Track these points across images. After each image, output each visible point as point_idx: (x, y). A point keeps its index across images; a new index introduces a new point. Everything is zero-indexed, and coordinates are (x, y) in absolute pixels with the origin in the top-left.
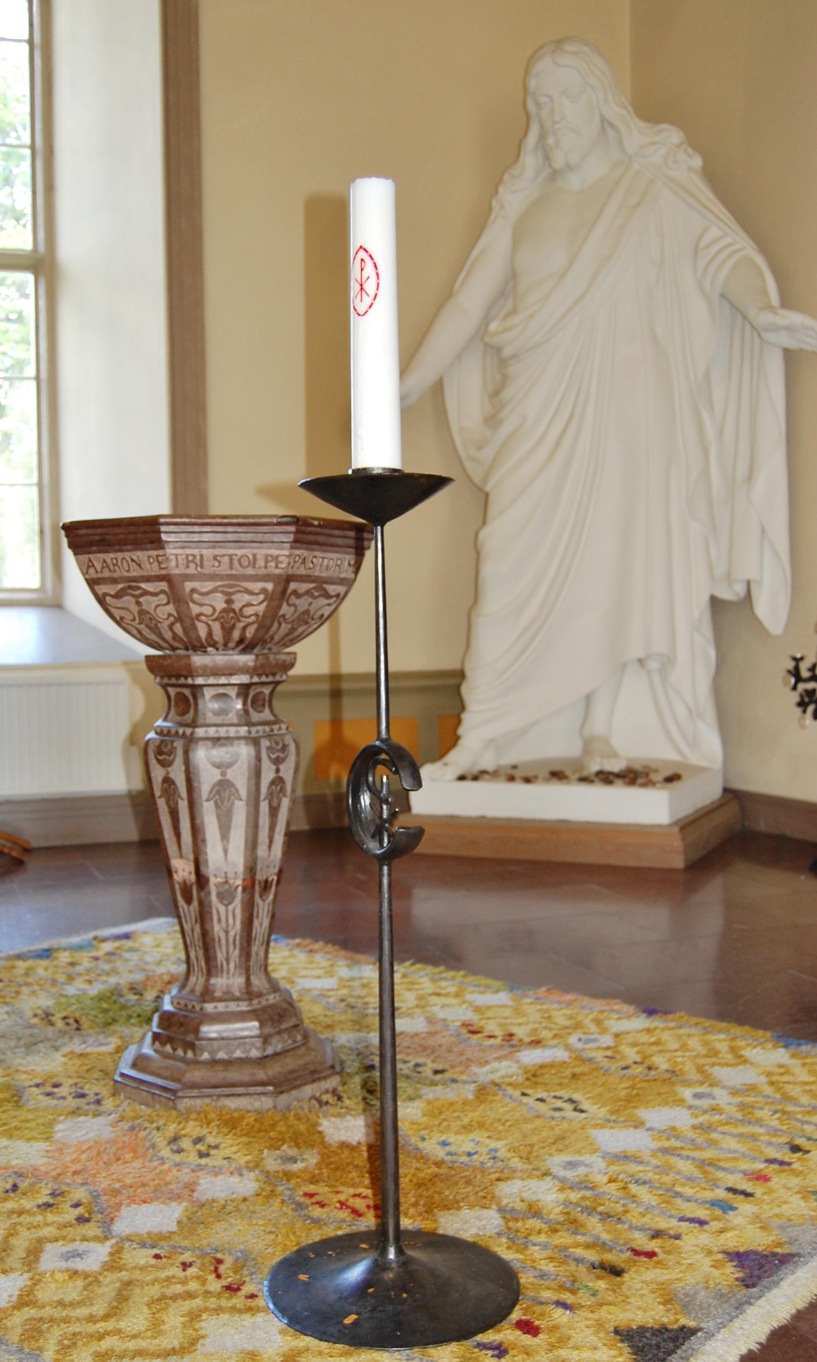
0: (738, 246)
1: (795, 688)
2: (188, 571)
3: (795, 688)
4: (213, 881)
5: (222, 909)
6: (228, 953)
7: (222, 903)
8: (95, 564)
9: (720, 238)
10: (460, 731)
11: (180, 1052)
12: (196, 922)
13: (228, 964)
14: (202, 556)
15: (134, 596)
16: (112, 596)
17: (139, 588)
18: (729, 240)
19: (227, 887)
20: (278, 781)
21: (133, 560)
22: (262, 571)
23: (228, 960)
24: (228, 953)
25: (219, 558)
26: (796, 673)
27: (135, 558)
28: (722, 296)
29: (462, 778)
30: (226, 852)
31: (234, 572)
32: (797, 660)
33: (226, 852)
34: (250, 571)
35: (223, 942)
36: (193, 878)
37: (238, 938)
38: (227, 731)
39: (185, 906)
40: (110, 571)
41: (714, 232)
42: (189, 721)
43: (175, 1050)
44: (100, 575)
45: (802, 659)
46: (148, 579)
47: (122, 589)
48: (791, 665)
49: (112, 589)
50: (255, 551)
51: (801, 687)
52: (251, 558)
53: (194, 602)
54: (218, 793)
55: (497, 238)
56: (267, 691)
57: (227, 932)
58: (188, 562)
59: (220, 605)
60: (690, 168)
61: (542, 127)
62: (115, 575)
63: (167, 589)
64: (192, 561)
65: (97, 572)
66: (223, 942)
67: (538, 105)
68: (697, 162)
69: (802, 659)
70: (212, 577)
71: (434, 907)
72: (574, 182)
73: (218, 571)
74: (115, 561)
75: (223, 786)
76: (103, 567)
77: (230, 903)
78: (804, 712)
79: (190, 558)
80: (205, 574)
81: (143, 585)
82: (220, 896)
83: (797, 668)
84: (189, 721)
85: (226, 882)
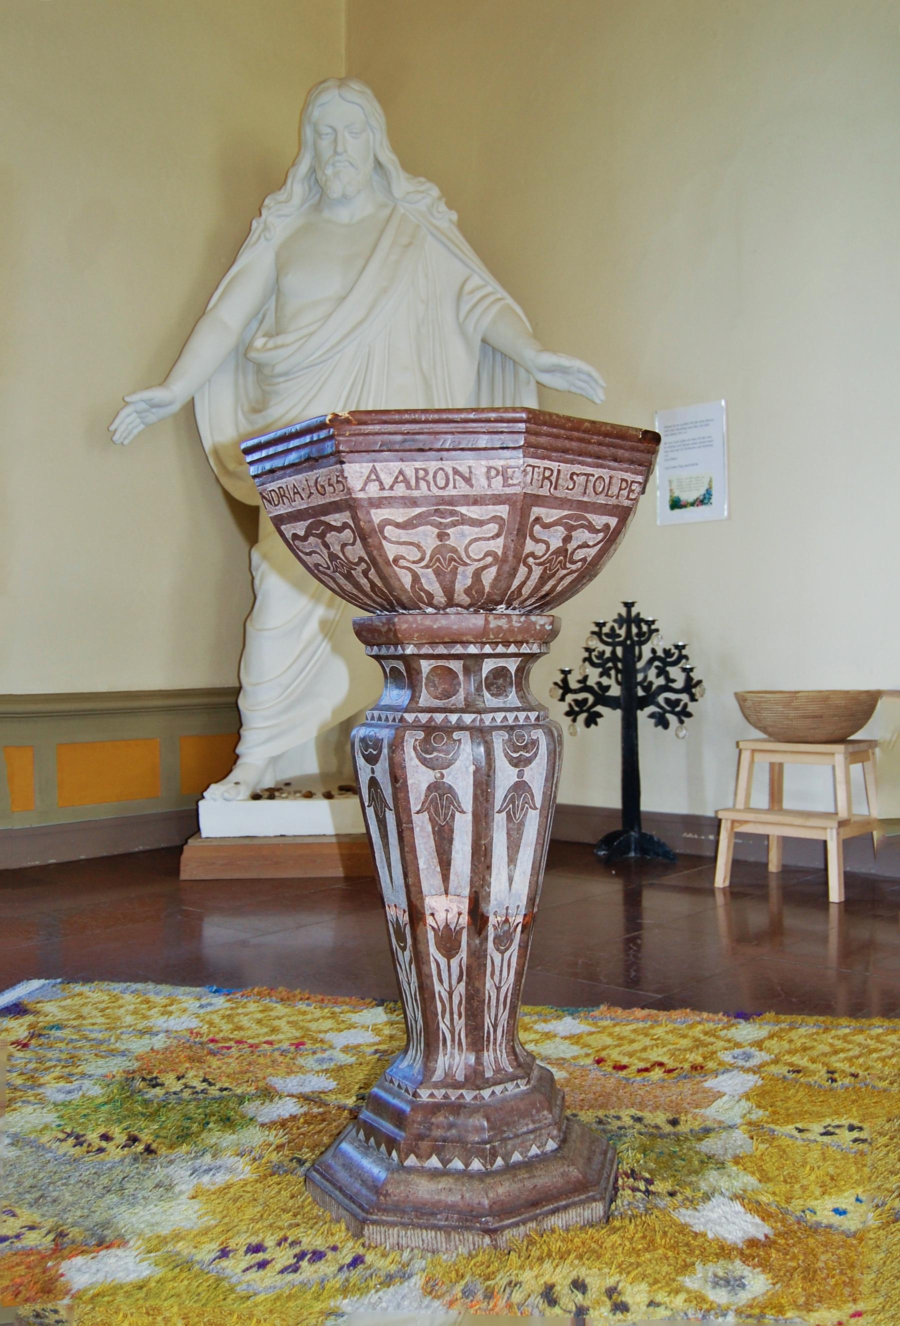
0: (499, 296)
1: (562, 699)
2: (541, 492)
3: (562, 699)
4: (492, 920)
5: (497, 957)
6: (496, 1016)
7: (498, 950)
8: (382, 476)
9: (483, 287)
10: (240, 750)
11: (476, 1165)
12: (459, 980)
13: (495, 1031)
14: (559, 471)
15: (439, 525)
16: (398, 525)
17: (453, 513)
18: (489, 289)
19: (506, 928)
20: (520, 787)
21: (456, 472)
22: (613, 501)
23: (495, 1027)
24: (496, 1016)
25: (575, 477)
26: (565, 688)
27: (463, 469)
28: (484, 341)
29: (256, 797)
30: (511, 880)
31: (585, 499)
32: (566, 673)
33: (511, 880)
34: (602, 500)
35: (494, 1002)
36: (464, 920)
37: (509, 994)
38: (493, 719)
39: (443, 961)
40: (409, 487)
41: (475, 281)
42: (462, 705)
43: (445, 1162)
44: (386, 494)
45: (570, 672)
46: (476, 501)
47: (419, 515)
48: (559, 678)
49: (300, 528)
50: (613, 473)
51: (570, 698)
52: (607, 481)
53: (533, 537)
54: (512, 801)
55: (257, 261)
56: (512, 665)
57: (498, 989)
58: (544, 478)
59: (556, 543)
60: (451, 221)
61: (317, 156)
62: (416, 493)
63: (505, 516)
64: (548, 478)
65: (382, 488)
66: (494, 1002)
67: (318, 134)
68: (454, 216)
69: (570, 672)
70: (562, 503)
71: (220, 933)
72: (343, 215)
73: (570, 495)
74: (421, 473)
75: (441, 797)
76: (396, 481)
77: (507, 949)
78: (574, 720)
79: (547, 474)
80: (556, 498)
81: (463, 510)
82: (498, 940)
83: (565, 681)
84: (462, 705)
85: (507, 921)
